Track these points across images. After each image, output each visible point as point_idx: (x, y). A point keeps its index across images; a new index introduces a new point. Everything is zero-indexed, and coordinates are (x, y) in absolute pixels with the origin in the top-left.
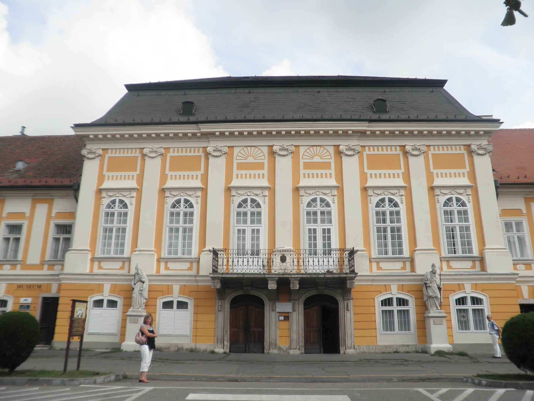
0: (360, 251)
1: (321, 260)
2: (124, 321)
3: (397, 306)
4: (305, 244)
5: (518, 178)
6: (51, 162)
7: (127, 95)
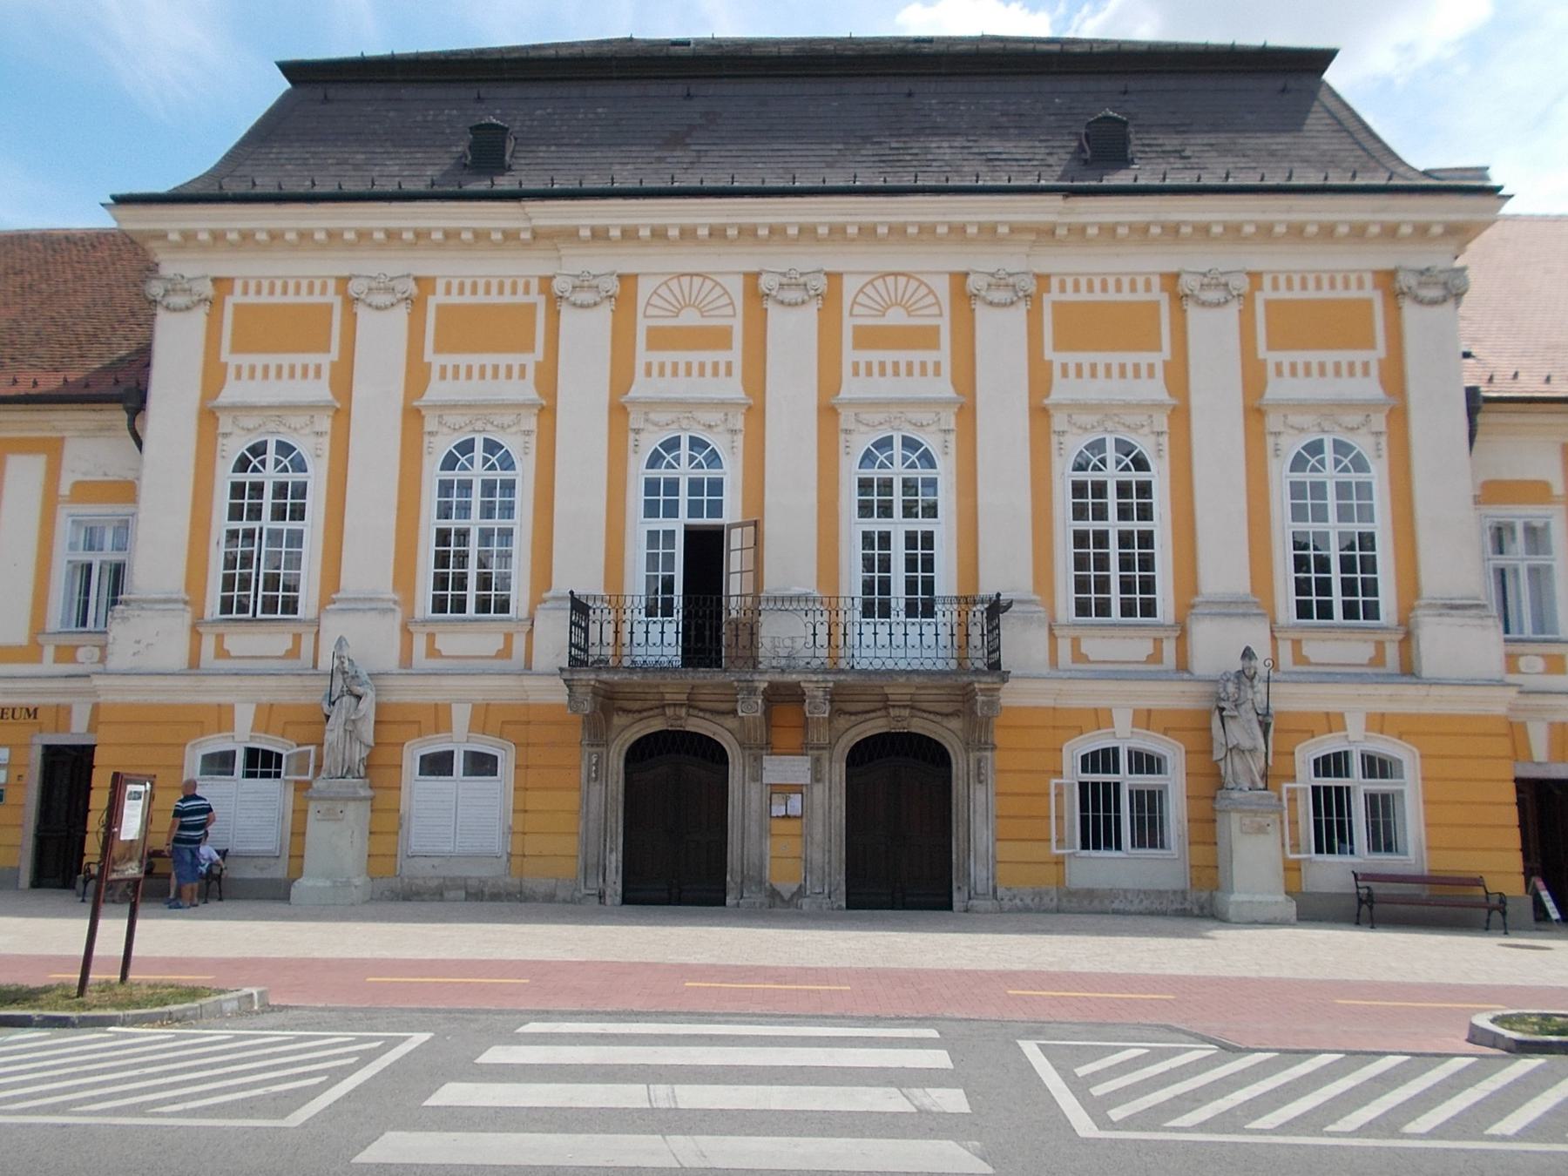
0: (1021, 602)
1: (898, 631)
2: (300, 814)
3: (1130, 772)
4: (852, 579)
5: (1548, 380)
6: (52, 318)
7: (286, 97)
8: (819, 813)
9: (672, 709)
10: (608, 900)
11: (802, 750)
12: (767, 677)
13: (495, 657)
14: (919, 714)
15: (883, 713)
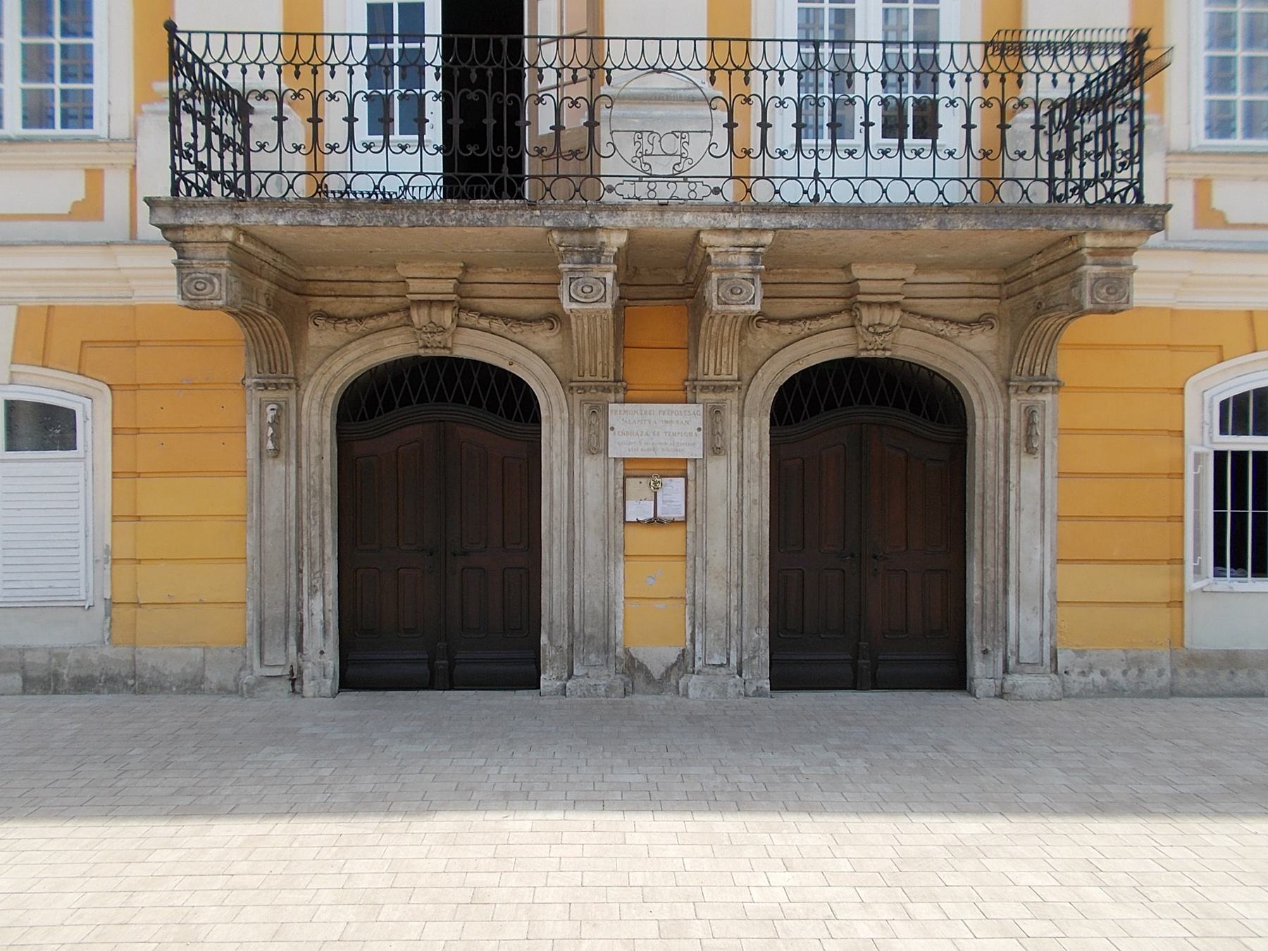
8: (718, 516)
9: (424, 311)
10: (309, 687)
11: (685, 392)
12: (627, 220)
13: (71, 216)
14: (915, 321)
15: (844, 319)
